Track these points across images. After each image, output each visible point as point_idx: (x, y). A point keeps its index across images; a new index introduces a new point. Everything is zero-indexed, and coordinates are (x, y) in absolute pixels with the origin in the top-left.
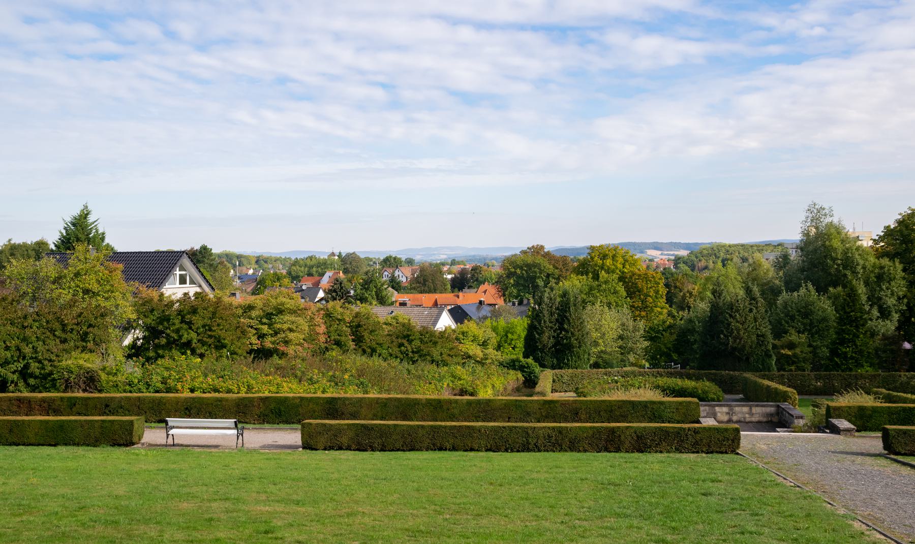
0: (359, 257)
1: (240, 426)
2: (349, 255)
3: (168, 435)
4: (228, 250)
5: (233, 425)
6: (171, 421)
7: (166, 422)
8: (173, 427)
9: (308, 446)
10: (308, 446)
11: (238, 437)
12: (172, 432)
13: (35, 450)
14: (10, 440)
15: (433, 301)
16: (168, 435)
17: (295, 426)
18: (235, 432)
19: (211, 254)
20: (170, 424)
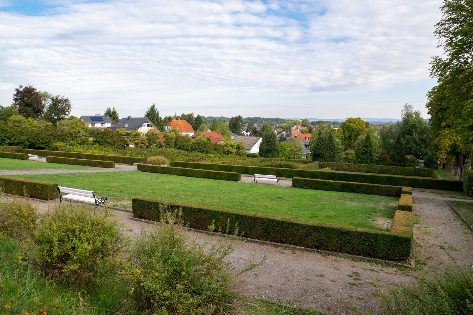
0: (423, 121)
1: (278, 178)
2: (350, 121)
3: (255, 180)
4: (278, 117)
5: (276, 178)
6: (256, 175)
7: (254, 175)
8: (256, 177)
9: (294, 186)
10: (294, 186)
11: (277, 182)
12: (256, 179)
13: (352, 200)
14: (196, 176)
15: (304, 137)
16: (255, 180)
17: (289, 179)
18: (276, 180)
19: (242, 119)
20: (255, 176)
